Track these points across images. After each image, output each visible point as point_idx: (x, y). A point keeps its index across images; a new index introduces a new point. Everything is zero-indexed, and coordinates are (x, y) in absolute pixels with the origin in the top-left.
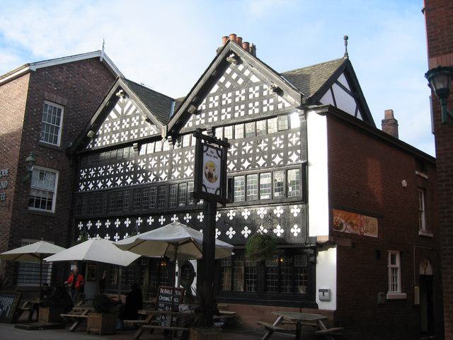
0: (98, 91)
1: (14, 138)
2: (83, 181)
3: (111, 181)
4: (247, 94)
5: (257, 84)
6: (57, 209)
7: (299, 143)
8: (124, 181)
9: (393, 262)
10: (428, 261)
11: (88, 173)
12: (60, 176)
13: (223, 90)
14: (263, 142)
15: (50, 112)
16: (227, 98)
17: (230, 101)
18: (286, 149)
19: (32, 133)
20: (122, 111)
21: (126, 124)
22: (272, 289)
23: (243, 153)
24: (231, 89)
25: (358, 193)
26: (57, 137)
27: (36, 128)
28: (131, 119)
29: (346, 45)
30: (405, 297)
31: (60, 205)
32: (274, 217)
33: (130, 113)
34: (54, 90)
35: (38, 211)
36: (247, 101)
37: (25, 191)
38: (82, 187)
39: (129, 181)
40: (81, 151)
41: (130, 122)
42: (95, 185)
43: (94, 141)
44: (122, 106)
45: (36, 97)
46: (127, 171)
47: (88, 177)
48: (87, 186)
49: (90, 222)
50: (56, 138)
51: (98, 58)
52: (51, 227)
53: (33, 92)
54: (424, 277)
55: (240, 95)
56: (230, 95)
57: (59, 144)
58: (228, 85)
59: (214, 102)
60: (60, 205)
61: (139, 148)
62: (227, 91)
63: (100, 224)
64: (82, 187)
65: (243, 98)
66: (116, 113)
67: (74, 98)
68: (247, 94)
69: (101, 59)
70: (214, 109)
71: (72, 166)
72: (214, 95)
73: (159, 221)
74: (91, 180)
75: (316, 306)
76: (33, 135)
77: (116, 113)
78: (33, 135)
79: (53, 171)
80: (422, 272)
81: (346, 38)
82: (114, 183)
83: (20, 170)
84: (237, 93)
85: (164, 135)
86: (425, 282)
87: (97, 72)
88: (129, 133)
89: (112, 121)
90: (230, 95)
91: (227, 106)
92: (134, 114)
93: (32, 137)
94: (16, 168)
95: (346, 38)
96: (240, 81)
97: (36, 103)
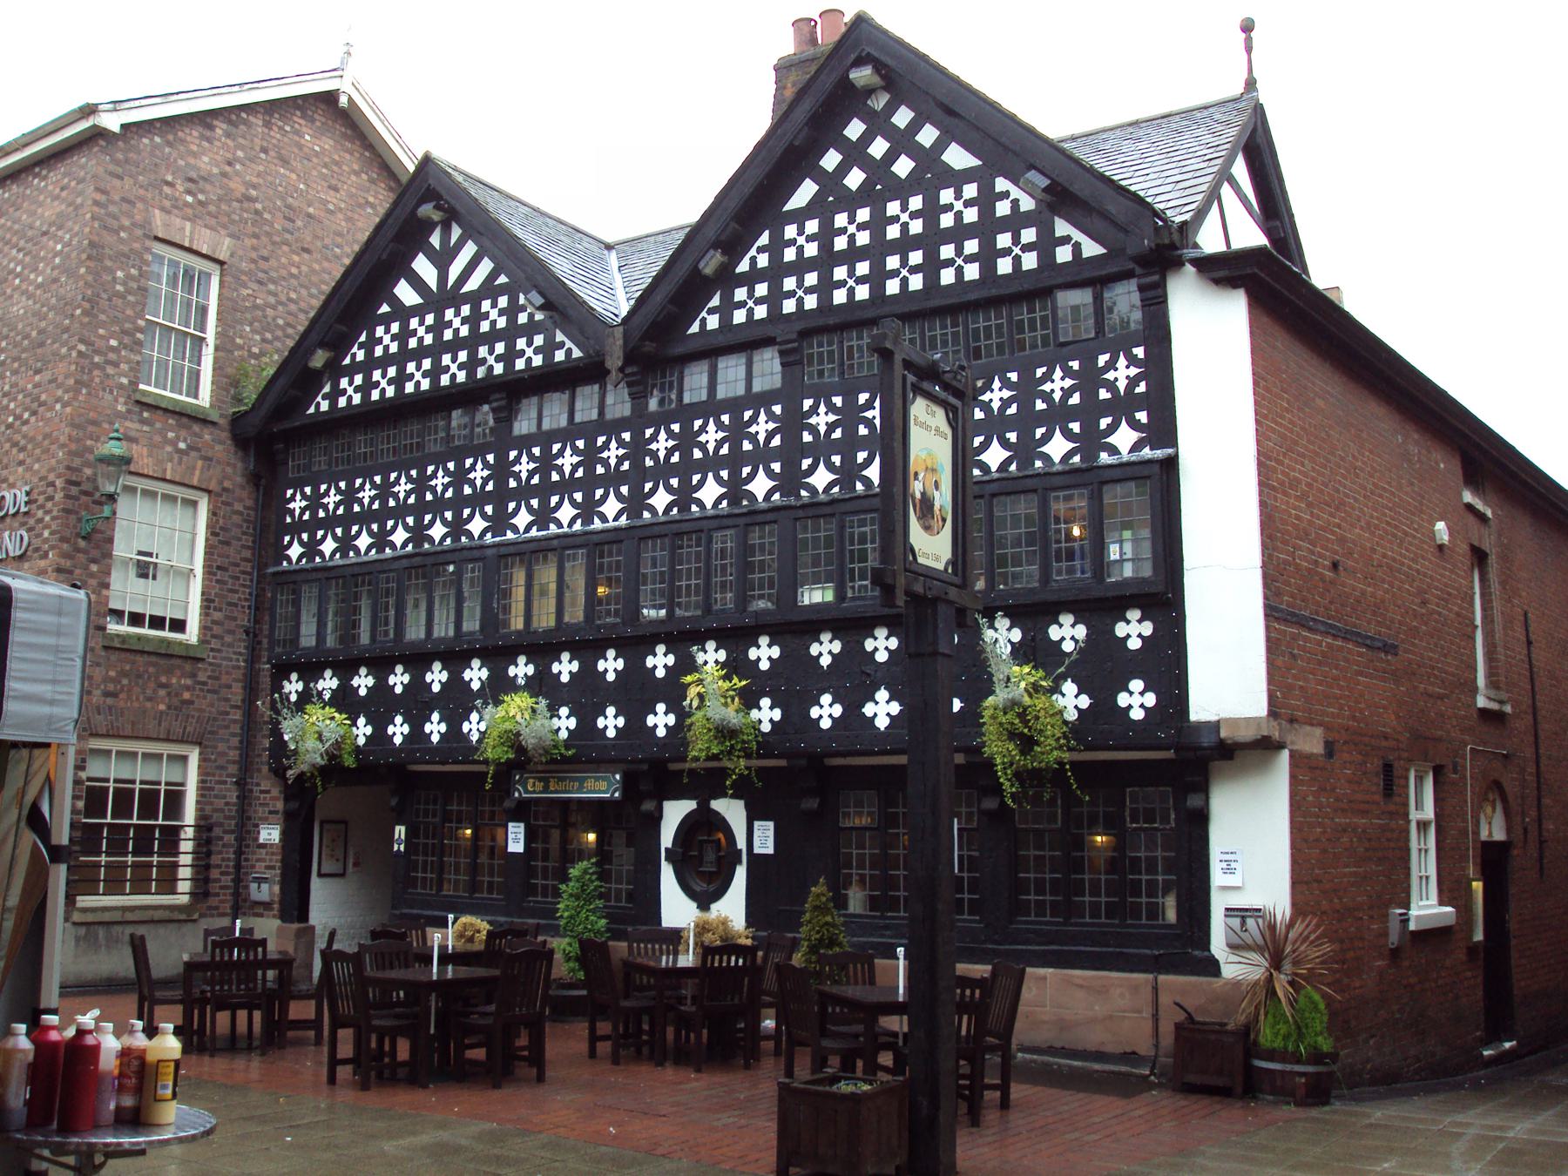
0: (331, 212)
1: (47, 375)
2: (297, 528)
3: (301, 543)
4: (931, 212)
5: (967, 176)
6: (204, 628)
7: (1142, 388)
8: (457, 528)
9: (1420, 805)
10: (1497, 797)
11: (315, 502)
12: (213, 513)
13: (832, 198)
14: (997, 384)
15: (173, 281)
16: (852, 229)
17: (863, 238)
18: (638, 476)
19: (112, 356)
20: (443, 278)
21: (456, 322)
22: (1040, 905)
23: (649, 462)
24: (866, 195)
25: (1335, 566)
26: (198, 373)
27: (127, 340)
28: (476, 308)
29: (1249, 49)
30: (1451, 921)
31: (217, 615)
32: (1088, 649)
33: (473, 284)
34: (186, 204)
35: (139, 638)
36: (931, 240)
37: (94, 568)
38: (295, 551)
39: (328, 546)
40: (287, 425)
41: (475, 319)
42: (346, 544)
43: (336, 384)
44: (442, 261)
45: (122, 228)
46: (467, 490)
47: (314, 514)
48: (312, 549)
49: (399, 669)
50: (195, 376)
51: (330, 98)
52: (186, 695)
53: (112, 209)
54: (1489, 847)
55: (905, 217)
56: (916, 203)
57: (205, 398)
58: (855, 179)
59: (801, 240)
60: (217, 615)
61: (506, 416)
62: (850, 202)
63: (370, 681)
64: (295, 551)
65: (811, 250)
66: (418, 284)
67: (256, 236)
68: (931, 212)
69: (343, 100)
70: (801, 266)
71: (255, 479)
72: (799, 217)
73: (391, 682)
74: (329, 523)
75: (1212, 967)
76: (116, 365)
77: (418, 284)
78: (116, 365)
79: (191, 494)
80: (1484, 835)
81: (1247, 27)
82: (418, 534)
83: (74, 490)
84: (893, 208)
85: (614, 361)
86: (1494, 860)
87: (328, 143)
88: (473, 355)
89: (402, 313)
90: (863, 215)
91: (853, 255)
92: (489, 289)
93: (110, 370)
94: (59, 483)
95: (1247, 27)
96: (903, 167)
97: (126, 249)
